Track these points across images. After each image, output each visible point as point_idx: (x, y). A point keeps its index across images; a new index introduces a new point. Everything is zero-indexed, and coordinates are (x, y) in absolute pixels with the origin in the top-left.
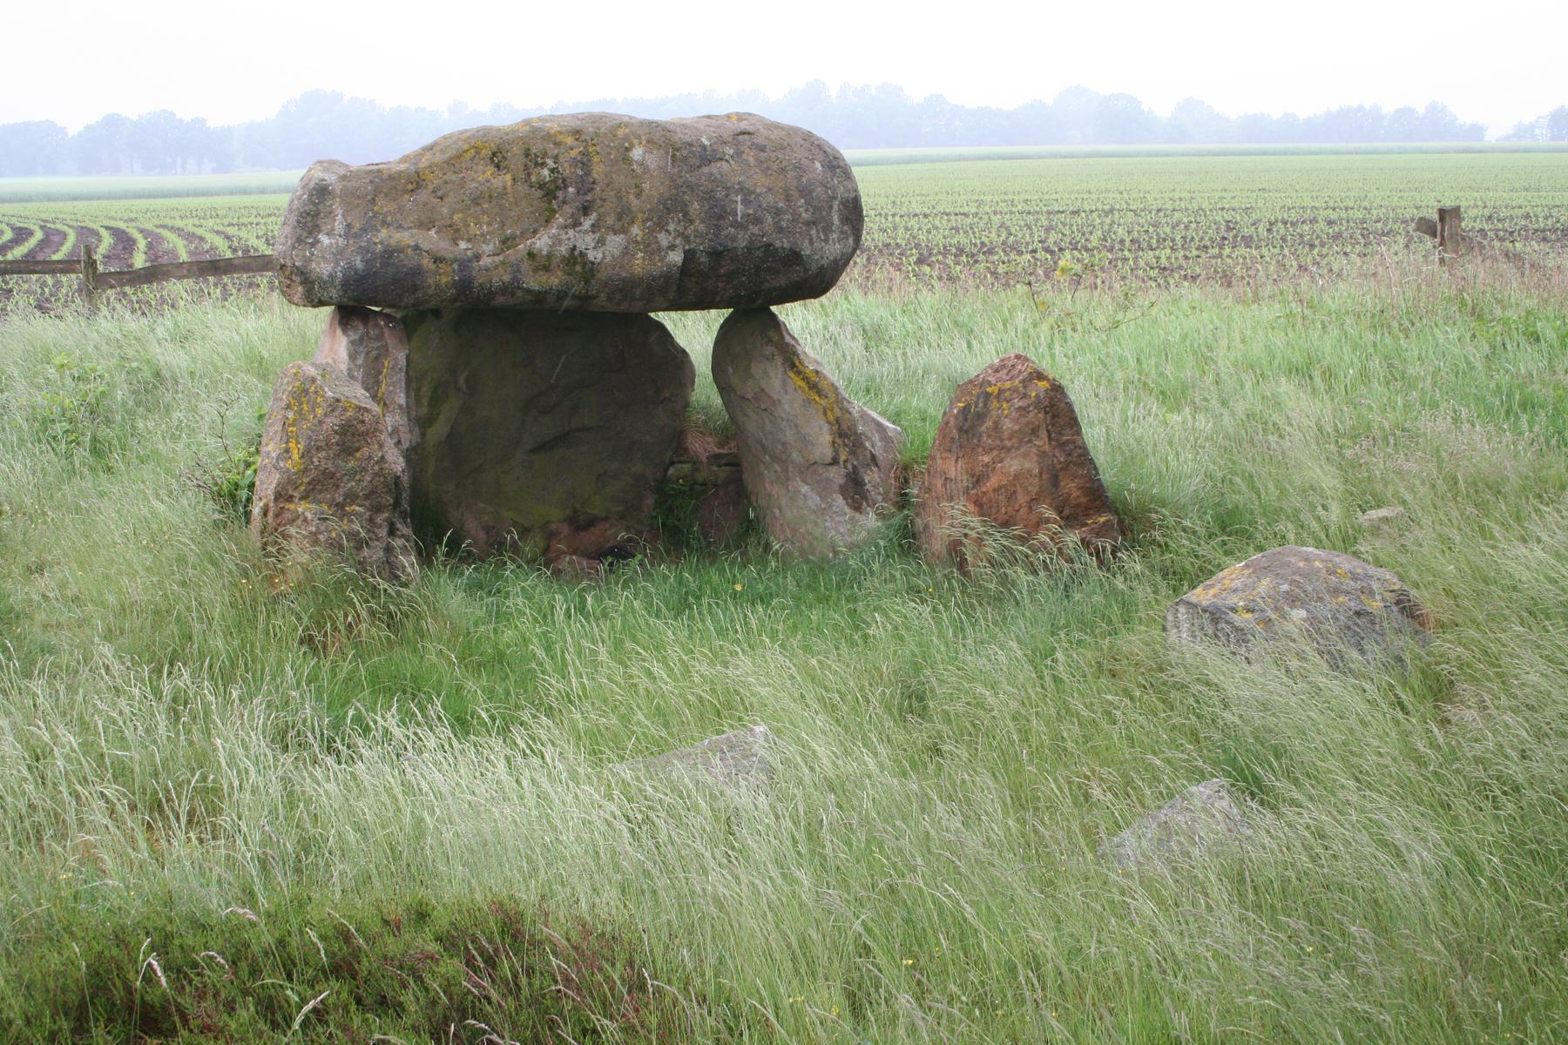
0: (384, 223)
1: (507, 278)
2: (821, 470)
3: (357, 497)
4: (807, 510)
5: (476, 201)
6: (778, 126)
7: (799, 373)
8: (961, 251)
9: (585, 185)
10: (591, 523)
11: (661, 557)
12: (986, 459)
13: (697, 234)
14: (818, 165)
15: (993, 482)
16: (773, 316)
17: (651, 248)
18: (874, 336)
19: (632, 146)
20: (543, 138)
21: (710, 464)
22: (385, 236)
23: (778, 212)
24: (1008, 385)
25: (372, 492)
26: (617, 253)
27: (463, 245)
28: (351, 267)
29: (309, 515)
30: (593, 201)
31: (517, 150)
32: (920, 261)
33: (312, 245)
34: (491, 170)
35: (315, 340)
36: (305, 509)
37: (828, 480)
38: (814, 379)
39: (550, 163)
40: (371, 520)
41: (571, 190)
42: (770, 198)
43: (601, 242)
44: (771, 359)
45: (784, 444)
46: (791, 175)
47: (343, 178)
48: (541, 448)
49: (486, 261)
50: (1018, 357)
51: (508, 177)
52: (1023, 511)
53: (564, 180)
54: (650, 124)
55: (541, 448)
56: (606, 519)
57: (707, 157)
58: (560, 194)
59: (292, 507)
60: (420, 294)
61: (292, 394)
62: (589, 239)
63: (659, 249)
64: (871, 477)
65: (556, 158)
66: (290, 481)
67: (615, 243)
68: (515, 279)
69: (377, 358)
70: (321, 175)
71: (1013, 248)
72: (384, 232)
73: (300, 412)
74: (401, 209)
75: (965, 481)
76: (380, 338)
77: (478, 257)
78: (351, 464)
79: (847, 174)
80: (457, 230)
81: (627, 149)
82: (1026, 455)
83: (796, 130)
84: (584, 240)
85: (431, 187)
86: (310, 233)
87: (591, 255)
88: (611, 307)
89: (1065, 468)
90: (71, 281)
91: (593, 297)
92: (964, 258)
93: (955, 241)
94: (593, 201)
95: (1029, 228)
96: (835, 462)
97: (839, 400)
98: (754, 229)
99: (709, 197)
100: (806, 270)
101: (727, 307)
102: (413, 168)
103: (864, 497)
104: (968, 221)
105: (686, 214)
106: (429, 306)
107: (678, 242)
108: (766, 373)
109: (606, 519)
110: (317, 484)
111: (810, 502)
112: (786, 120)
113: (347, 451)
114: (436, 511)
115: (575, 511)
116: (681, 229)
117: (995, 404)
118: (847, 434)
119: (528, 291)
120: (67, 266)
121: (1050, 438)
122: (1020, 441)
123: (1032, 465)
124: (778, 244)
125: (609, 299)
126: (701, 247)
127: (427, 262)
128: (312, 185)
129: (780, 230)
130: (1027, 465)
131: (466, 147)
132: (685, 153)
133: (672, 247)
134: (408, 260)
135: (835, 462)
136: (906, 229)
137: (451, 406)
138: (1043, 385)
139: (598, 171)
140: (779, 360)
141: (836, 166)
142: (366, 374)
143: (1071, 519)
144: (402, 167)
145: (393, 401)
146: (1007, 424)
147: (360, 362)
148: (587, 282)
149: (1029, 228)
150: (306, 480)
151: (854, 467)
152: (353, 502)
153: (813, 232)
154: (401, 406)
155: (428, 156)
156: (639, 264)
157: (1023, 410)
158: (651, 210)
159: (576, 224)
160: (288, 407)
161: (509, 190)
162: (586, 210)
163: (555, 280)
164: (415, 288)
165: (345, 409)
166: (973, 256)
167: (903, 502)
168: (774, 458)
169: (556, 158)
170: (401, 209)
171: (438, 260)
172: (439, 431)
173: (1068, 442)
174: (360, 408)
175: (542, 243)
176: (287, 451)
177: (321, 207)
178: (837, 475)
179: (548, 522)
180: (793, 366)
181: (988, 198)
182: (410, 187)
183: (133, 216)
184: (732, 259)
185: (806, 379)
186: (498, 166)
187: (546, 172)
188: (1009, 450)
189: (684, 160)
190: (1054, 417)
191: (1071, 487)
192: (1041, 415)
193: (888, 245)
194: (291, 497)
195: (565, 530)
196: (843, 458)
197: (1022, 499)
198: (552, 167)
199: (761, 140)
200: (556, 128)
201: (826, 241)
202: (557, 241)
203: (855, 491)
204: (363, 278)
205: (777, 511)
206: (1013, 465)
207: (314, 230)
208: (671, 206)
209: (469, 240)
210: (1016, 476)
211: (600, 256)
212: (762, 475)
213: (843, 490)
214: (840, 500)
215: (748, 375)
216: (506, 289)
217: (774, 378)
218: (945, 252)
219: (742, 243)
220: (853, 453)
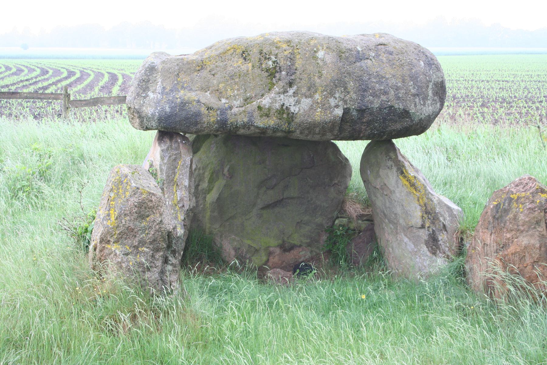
0: (183, 87)
1: (246, 120)
2: (415, 230)
4: (406, 251)
5: (232, 77)
6: (401, 41)
7: (405, 177)
8: (504, 100)
9: (291, 71)
10: (292, 248)
11: (324, 277)
12: (508, 235)
13: (351, 99)
14: (422, 63)
15: (512, 249)
16: (393, 145)
18: (451, 153)
19: (318, 50)
20: (270, 44)
21: (358, 219)
22: (183, 95)
23: (398, 89)
24: (523, 194)
25: (154, 240)
26: (306, 108)
28: (163, 109)
29: (118, 252)
31: (256, 50)
32: (483, 105)
33: (145, 98)
34: (241, 60)
35: (149, 148)
36: (114, 248)
38: (413, 181)
40: (153, 256)
41: (283, 73)
43: (298, 102)
44: (390, 168)
45: (395, 214)
46: (406, 68)
47: (163, 62)
48: (267, 207)
49: (235, 110)
50: (530, 179)
51: (250, 65)
52: (529, 267)
53: (280, 68)
54: (330, 39)
55: (267, 207)
56: (300, 246)
57: (360, 57)
58: (277, 75)
59: (109, 246)
60: (199, 126)
61: (114, 183)
62: (292, 100)
63: (330, 107)
64: (442, 237)
65: (276, 56)
66: (108, 232)
67: (306, 103)
68: (250, 120)
69: (175, 160)
70: (153, 60)
71: (530, 100)
72: (182, 92)
73: (117, 194)
74: (192, 80)
75: (494, 247)
76: (177, 148)
77: (231, 108)
79: (438, 68)
82: (532, 236)
83: (411, 43)
84: (289, 101)
85: (209, 69)
86: (144, 91)
87: (292, 109)
88: (302, 137)
90: (57, 105)
91: (292, 132)
92: (505, 104)
93: (501, 95)
95: (539, 89)
96: (423, 227)
97: (427, 194)
98: (384, 98)
99: (359, 79)
100: (412, 121)
101: (367, 139)
102: (200, 58)
103: (438, 247)
104: (509, 85)
105: (346, 88)
106: (205, 133)
107: (340, 103)
108: (387, 176)
109: (300, 246)
110: (124, 235)
111: (408, 247)
112: (407, 38)
113: (142, 217)
115: (284, 241)
117: (515, 205)
118: (430, 212)
119: (257, 127)
120: (55, 96)
122: (529, 227)
124: (396, 106)
125: (301, 133)
126: (353, 106)
127: (203, 110)
128: (147, 66)
129: (398, 98)
130: (532, 242)
131: (229, 48)
132: (347, 54)
133: (337, 106)
134: (193, 108)
135: (423, 227)
136: (478, 88)
137: (220, 183)
139: (299, 63)
140: (395, 169)
141: (432, 63)
142: (169, 168)
144: (194, 58)
145: (182, 184)
146: (521, 217)
147: (165, 161)
149: (539, 89)
150: (118, 232)
151: (433, 231)
152: (143, 246)
153: (417, 100)
154: (185, 186)
155: (209, 52)
156: (319, 116)
157: (532, 210)
158: (326, 86)
160: (111, 190)
161: (250, 72)
162: (291, 84)
163: (272, 122)
164: (196, 123)
165: (142, 194)
166: (510, 103)
167: (460, 251)
168: (390, 222)
169: (276, 56)
170: (192, 80)
171: (209, 108)
172: (212, 197)
174: (150, 193)
175: (266, 101)
176: (109, 215)
177: (150, 77)
178: (424, 234)
179: (269, 247)
180: (402, 173)
181: (519, 73)
182: (198, 68)
183: (123, 68)
185: (409, 181)
186: (245, 59)
187: (270, 63)
188: (522, 232)
189: (347, 58)
192: (542, 214)
193: (467, 96)
194: (109, 241)
195: (278, 251)
196: (427, 225)
197: (528, 260)
198: (274, 63)
199: (390, 49)
201: (424, 105)
202: (274, 100)
203: (433, 243)
204: (169, 116)
205: (391, 249)
206: (524, 240)
207: (146, 89)
208: (338, 83)
209: (227, 98)
210: (526, 247)
211: (297, 110)
212: (383, 229)
213: (427, 243)
214: (425, 248)
215: (378, 176)
216: (245, 126)
217: (391, 178)
218: (496, 101)
219: (376, 105)
220: (433, 223)
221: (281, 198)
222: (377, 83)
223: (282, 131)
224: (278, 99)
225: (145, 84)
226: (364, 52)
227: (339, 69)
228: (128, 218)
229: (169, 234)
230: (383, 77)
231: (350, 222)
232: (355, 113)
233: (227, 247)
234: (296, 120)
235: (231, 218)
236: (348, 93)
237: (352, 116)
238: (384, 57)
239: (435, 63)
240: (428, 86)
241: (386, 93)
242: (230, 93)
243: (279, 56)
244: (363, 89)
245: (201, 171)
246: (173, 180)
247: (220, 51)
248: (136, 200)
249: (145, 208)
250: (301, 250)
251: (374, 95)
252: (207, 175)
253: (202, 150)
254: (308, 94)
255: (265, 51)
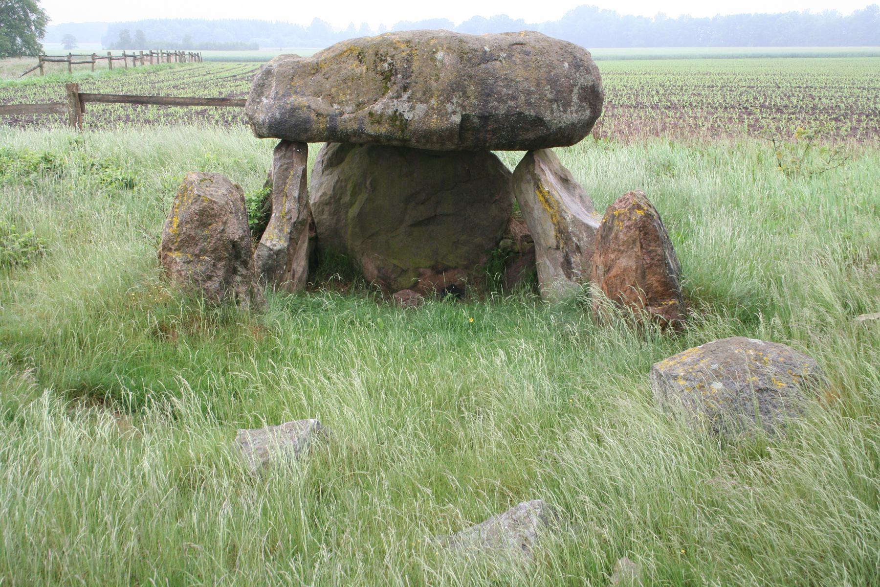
0: (296, 92)
1: (356, 127)
3: (207, 252)
5: (344, 81)
7: (541, 192)
9: (407, 74)
14: (566, 65)
17: (442, 113)
19: (437, 51)
21: (522, 241)
23: (529, 93)
25: (215, 249)
26: (422, 115)
27: (335, 106)
29: (178, 260)
30: (410, 83)
33: (258, 103)
34: (357, 62)
37: (556, 259)
39: (389, 59)
40: (214, 265)
41: (399, 76)
42: (526, 85)
43: (412, 108)
44: (529, 182)
49: (346, 116)
50: (632, 194)
56: (455, 268)
57: (486, 58)
60: (309, 134)
62: (406, 106)
63: (447, 113)
65: (393, 57)
66: (170, 240)
67: (421, 108)
68: (360, 127)
69: (286, 169)
74: (306, 84)
77: (341, 114)
78: (206, 232)
80: (333, 98)
81: (434, 53)
84: (402, 106)
86: (259, 96)
87: (406, 116)
89: (650, 266)
94: (410, 83)
96: (558, 248)
98: (511, 103)
99: (483, 82)
100: (548, 129)
105: (465, 93)
107: (458, 110)
110: (185, 242)
113: (204, 225)
114: (330, 261)
116: (460, 102)
119: (369, 135)
121: (642, 247)
122: (628, 248)
123: (632, 264)
124: (527, 113)
125: (417, 142)
127: (313, 116)
129: (529, 104)
132: (470, 55)
133: (454, 113)
134: (303, 114)
135: (558, 248)
137: (363, 197)
138: (640, 213)
139: (416, 65)
140: (532, 184)
141: (580, 63)
143: (652, 300)
145: (291, 194)
148: (403, 131)
150: (179, 240)
152: (204, 254)
154: (295, 198)
156: (434, 122)
159: (399, 96)
160: (177, 197)
161: (364, 75)
162: (405, 88)
163: (384, 129)
165: (203, 201)
169: (393, 57)
170: (306, 84)
171: (319, 115)
172: (353, 211)
173: (653, 251)
175: (378, 107)
178: (559, 256)
179: (418, 268)
180: (538, 188)
182: (313, 71)
184: (496, 121)
186: (360, 61)
187: (386, 65)
188: (622, 252)
190: (645, 234)
191: (653, 280)
192: (637, 232)
198: (387, 63)
199: (527, 48)
200: (398, 39)
202: (387, 106)
204: (279, 123)
208: (457, 87)
209: (339, 104)
211: (411, 116)
216: (356, 133)
219: (502, 110)
220: (566, 244)
221: (433, 214)
222: (504, 87)
223: (396, 139)
224: (391, 104)
225: (260, 89)
226: (493, 52)
227: (458, 72)
228: (189, 226)
229: (234, 244)
230: (512, 80)
231: (514, 243)
232: (476, 120)
233: (370, 266)
234: (410, 128)
235: (373, 235)
236: (468, 98)
237: (473, 123)
238: (517, 58)
239: (586, 64)
240: (572, 91)
241: (514, 98)
242: (342, 97)
243: (396, 58)
244: (487, 93)
245: (343, 184)
246: (282, 191)
247: (337, 52)
248: (197, 207)
249: (207, 216)
250: (456, 272)
251: (500, 100)
252: (350, 187)
253: (347, 160)
254: (423, 98)
255: (381, 52)
